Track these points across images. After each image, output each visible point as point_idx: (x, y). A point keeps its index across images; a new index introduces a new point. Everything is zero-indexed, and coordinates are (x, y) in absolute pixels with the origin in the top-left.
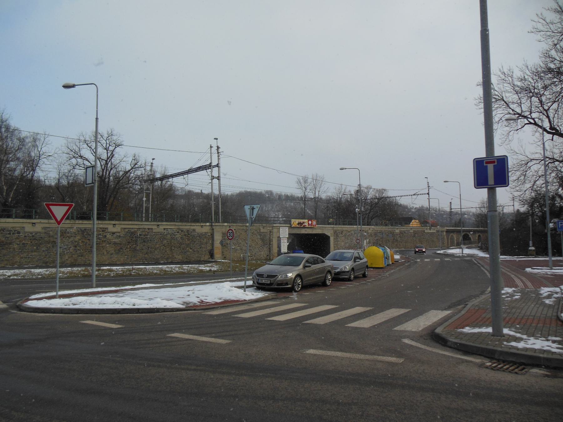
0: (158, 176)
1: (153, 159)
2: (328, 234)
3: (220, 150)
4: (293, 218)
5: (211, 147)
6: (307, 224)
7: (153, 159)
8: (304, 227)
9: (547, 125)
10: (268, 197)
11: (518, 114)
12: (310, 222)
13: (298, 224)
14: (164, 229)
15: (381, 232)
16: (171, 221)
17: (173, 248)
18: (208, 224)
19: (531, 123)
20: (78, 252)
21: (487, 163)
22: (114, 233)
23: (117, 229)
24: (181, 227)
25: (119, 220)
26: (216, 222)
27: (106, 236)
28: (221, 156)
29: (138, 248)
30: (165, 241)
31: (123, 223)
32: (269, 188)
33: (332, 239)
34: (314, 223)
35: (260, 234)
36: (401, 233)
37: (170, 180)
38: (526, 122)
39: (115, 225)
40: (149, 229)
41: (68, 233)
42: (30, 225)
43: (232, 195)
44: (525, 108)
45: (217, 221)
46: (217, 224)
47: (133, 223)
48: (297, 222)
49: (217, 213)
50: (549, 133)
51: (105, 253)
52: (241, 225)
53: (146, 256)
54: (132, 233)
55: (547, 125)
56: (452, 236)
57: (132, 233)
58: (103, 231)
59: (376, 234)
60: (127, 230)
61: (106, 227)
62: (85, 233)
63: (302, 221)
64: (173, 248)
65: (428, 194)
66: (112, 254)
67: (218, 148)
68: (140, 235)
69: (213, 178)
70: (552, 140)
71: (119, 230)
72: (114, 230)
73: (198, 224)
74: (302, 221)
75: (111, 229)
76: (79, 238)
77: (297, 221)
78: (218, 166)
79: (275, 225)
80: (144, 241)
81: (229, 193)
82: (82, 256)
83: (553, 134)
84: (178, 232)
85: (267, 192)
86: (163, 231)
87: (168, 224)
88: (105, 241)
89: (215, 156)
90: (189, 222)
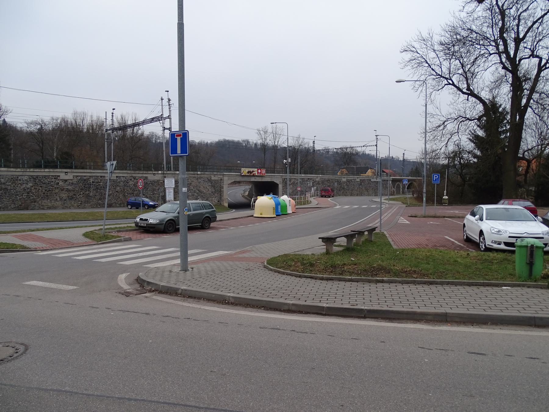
0: (130, 122)
1: (114, 109)
2: (277, 181)
3: (171, 102)
4: (244, 167)
5: (162, 99)
6: (256, 173)
7: (114, 109)
8: (254, 176)
9: (464, 86)
10: (246, 146)
11: (439, 75)
12: (259, 171)
13: (248, 172)
14: (117, 177)
15: (328, 180)
16: (122, 170)
17: (126, 194)
18: (160, 172)
19: (450, 84)
20: (32, 198)
21: (177, 136)
22: (66, 181)
23: (70, 177)
24: (134, 175)
25: (71, 168)
26: (168, 170)
27: (58, 183)
28: (172, 109)
29: (91, 194)
30: (118, 188)
31: (74, 171)
32: (245, 138)
33: (280, 186)
34: (264, 171)
35: (210, 180)
36: (348, 181)
37: (141, 127)
38: (446, 83)
39: (67, 172)
40: (101, 177)
41: (20, 180)
42: (64, 174)
43: (211, 143)
44: (445, 69)
45: (169, 169)
46: (168, 172)
47: (85, 171)
48: (247, 171)
49: (168, 163)
50: (464, 93)
51: (59, 199)
52: (192, 173)
53: (100, 201)
54: (84, 181)
55: (464, 86)
56: (398, 185)
57: (85, 180)
58: (55, 178)
59: (323, 182)
60: (79, 178)
61: (58, 174)
62: (37, 181)
63: (251, 170)
64: (126, 194)
65: (376, 145)
66: (65, 200)
67: (169, 100)
68: (93, 182)
69: (164, 129)
70: (468, 100)
71: (71, 178)
72: (66, 177)
73: (150, 172)
74: (251, 170)
75: (63, 176)
76: (31, 185)
77: (247, 170)
78: (169, 117)
79: (225, 173)
80: (97, 188)
81: (209, 142)
82: (35, 202)
83: (468, 94)
84: (131, 180)
85: (244, 141)
86: (115, 178)
87: (122, 172)
88: (58, 188)
89: (166, 109)
90: (141, 170)
